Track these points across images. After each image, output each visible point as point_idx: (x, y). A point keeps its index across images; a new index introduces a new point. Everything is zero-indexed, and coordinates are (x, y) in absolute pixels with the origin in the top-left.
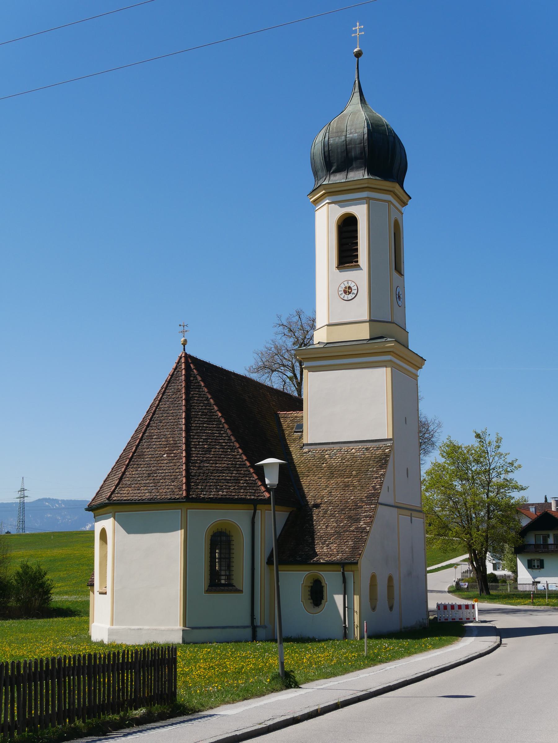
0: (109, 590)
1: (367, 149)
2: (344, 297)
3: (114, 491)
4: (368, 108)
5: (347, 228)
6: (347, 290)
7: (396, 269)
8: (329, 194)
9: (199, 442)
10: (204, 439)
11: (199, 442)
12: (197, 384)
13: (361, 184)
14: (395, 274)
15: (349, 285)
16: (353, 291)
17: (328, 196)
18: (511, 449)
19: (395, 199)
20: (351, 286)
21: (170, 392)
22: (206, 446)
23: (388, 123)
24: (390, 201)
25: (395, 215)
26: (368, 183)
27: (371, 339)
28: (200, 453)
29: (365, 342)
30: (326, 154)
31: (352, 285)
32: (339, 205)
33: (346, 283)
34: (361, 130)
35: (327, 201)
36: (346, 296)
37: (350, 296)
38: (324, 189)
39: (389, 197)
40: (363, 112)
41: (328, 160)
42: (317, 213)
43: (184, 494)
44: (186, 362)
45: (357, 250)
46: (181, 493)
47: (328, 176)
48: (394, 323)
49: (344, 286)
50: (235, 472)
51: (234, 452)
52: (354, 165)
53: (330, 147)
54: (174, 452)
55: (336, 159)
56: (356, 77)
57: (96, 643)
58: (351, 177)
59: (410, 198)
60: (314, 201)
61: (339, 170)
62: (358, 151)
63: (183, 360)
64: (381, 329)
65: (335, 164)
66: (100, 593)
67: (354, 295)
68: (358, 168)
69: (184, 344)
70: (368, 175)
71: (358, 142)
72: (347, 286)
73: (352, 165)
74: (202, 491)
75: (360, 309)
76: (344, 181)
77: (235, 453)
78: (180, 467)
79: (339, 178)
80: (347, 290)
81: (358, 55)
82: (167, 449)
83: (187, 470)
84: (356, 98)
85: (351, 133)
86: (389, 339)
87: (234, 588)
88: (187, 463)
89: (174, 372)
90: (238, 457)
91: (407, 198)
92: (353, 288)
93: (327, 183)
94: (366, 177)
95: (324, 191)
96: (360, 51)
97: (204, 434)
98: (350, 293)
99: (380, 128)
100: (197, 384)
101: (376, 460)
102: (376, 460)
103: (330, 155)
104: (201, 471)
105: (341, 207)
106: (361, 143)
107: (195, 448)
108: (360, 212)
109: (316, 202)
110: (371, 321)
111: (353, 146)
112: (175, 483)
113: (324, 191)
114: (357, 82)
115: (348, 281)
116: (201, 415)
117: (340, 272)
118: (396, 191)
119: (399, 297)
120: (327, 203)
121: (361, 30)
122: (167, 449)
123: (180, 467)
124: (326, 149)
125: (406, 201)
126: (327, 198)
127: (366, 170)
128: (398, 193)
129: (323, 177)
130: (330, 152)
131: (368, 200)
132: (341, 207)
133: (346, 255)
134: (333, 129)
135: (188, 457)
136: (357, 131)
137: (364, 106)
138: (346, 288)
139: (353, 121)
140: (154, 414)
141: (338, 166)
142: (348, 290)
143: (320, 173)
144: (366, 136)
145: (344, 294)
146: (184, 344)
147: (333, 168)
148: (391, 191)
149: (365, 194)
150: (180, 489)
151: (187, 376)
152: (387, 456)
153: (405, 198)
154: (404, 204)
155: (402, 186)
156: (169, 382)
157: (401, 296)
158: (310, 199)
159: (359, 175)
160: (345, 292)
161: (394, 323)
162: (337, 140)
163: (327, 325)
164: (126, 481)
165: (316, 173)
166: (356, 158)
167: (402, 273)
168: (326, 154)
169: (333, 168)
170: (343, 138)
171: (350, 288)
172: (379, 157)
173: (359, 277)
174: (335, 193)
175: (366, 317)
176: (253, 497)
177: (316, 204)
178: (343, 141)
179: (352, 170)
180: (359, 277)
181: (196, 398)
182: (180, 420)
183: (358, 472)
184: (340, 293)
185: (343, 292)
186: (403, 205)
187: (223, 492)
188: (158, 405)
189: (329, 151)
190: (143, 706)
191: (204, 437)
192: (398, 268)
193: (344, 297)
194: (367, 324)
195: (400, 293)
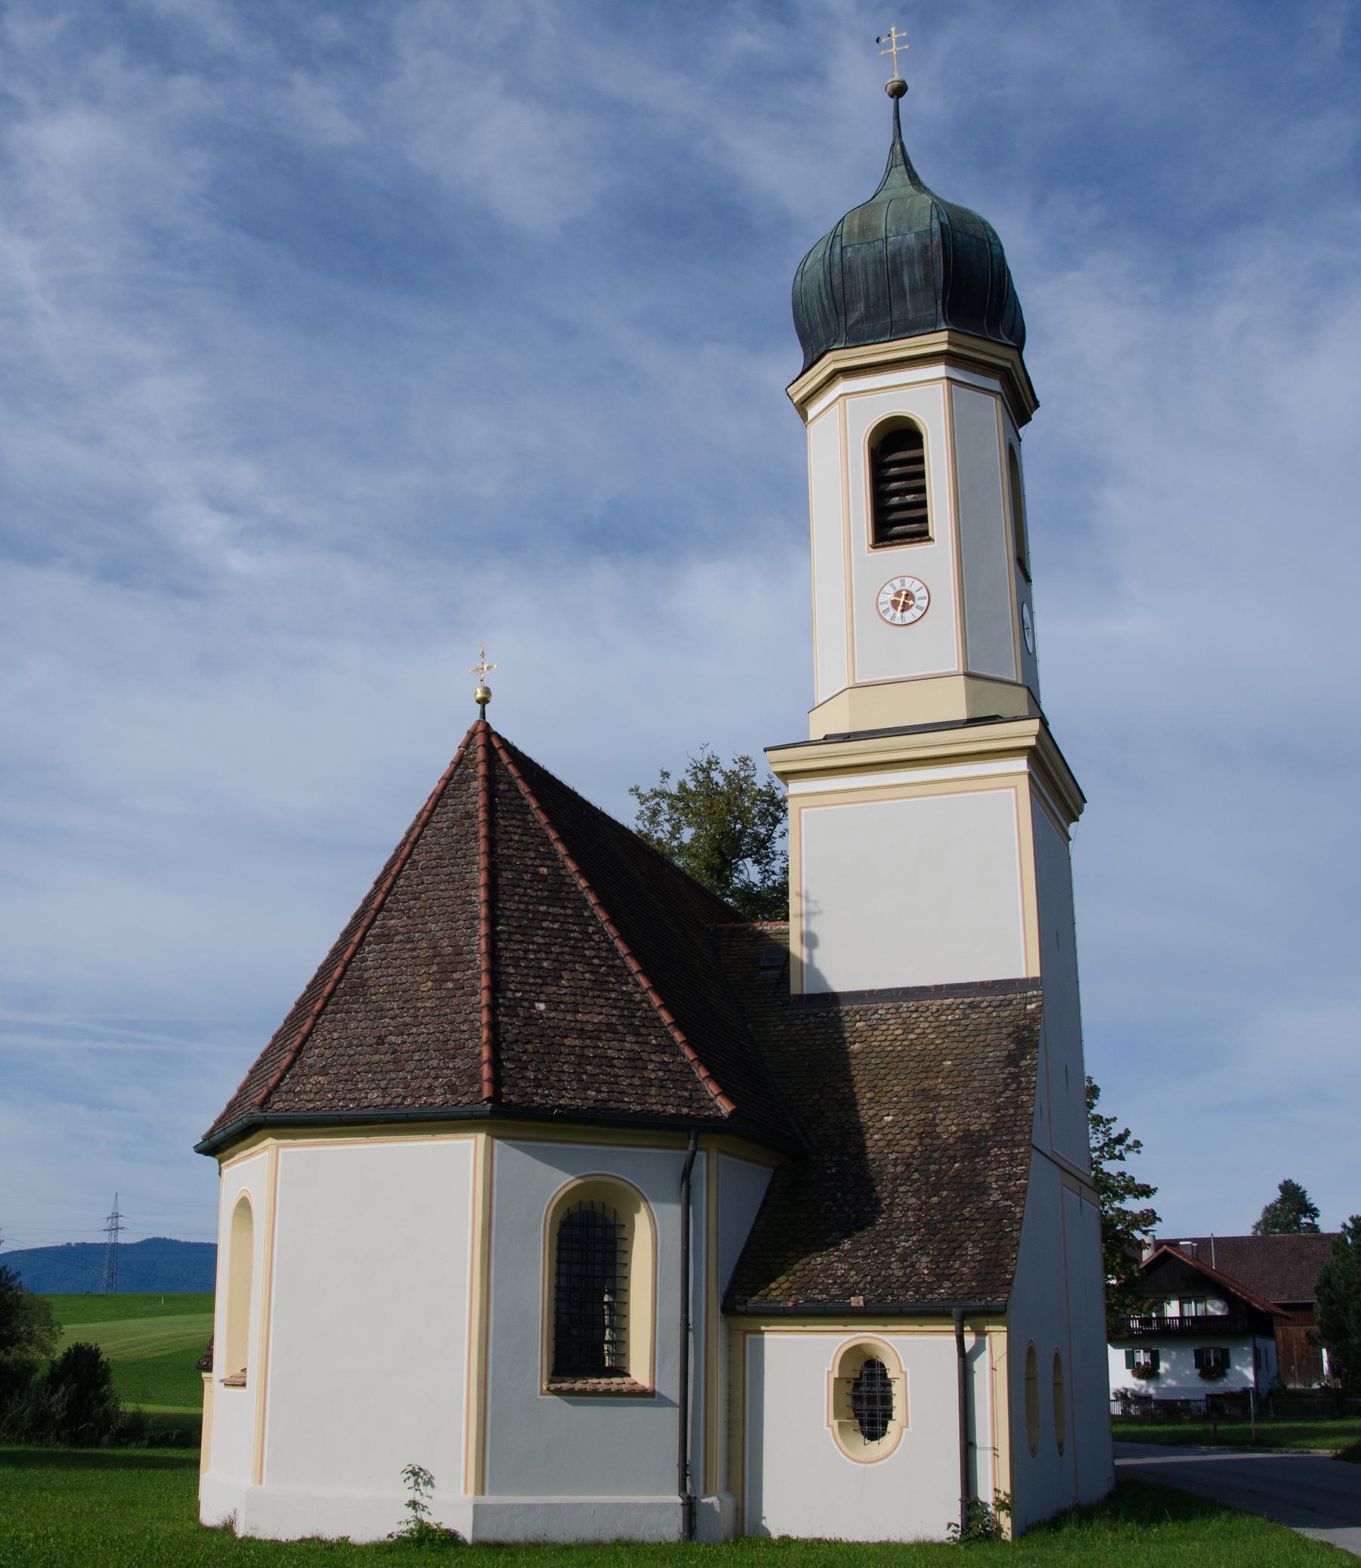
0: (252, 1378)
3: (277, 1085)
5: (895, 446)
9: (526, 951)
10: (539, 944)
11: (526, 951)
12: (518, 802)
15: (907, 586)
20: (913, 590)
21: (442, 821)
22: (545, 964)
28: (531, 980)
31: (913, 586)
33: (897, 583)
43: (487, 1091)
44: (488, 747)
46: (476, 1088)
50: (629, 1038)
51: (627, 983)
54: (456, 976)
57: (212, 1530)
63: (479, 740)
66: (229, 1384)
69: (484, 702)
74: (537, 1087)
75: (938, 643)
77: (630, 988)
78: (471, 1017)
82: (435, 968)
83: (494, 1026)
87: (626, 1379)
88: (493, 1007)
89: (455, 770)
90: (638, 997)
92: (917, 595)
97: (540, 932)
100: (518, 802)
101: (1004, 1031)
102: (1004, 1031)
104: (535, 1030)
107: (516, 967)
112: (458, 1062)
115: (902, 578)
116: (531, 881)
121: (900, 42)
122: (435, 968)
123: (471, 1017)
133: (896, 516)
135: (495, 988)
140: (397, 877)
142: (904, 601)
146: (484, 702)
150: (474, 1078)
151: (491, 780)
152: (1033, 1017)
156: (439, 799)
164: (311, 1058)
172: (967, 297)
173: (931, 564)
175: (956, 665)
176: (685, 1110)
181: (516, 837)
182: (473, 892)
183: (957, 1062)
184: (882, 608)
185: (889, 605)
187: (599, 1091)
188: (409, 855)
190: (1335, 1241)
191: (541, 941)
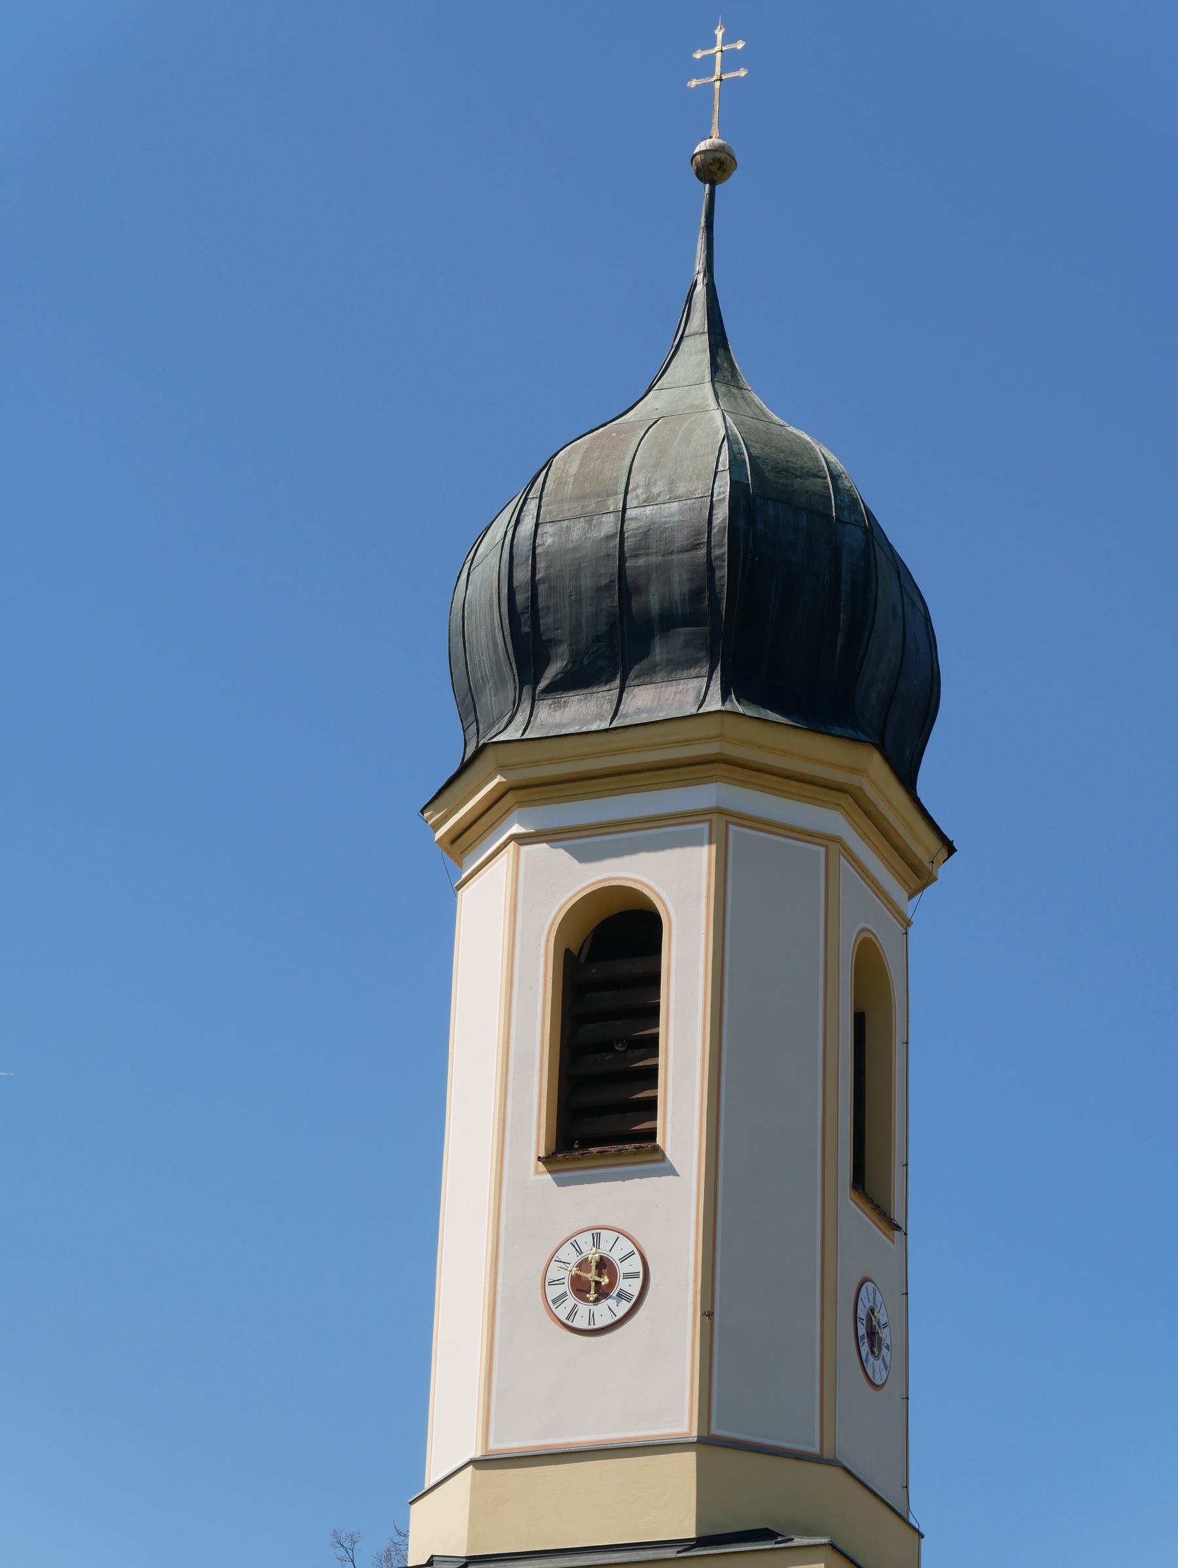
1: (722, 573)
2: (573, 1312)
4: (749, 402)
5: (607, 965)
6: (591, 1276)
7: (859, 1180)
8: (524, 791)
13: (688, 742)
14: (853, 1214)
15: (604, 1249)
16: (622, 1284)
17: (521, 803)
18: (570, 531)
19: (864, 836)
20: (615, 1256)
23: (840, 467)
24: (837, 840)
25: (860, 915)
26: (721, 737)
27: (702, 1541)
29: (671, 1553)
30: (521, 598)
32: (573, 852)
33: (585, 1241)
34: (700, 487)
35: (516, 829)
36: (583, 1309)
37: (604, 1313)
38: (502, 768)
39: (831, 820)
40: (718, 415)
41: (525, 629)
42: (467, 898)
45: (650, 1076)
47: (526, 706)
48: (833, 1463)
49: (574, 1259)
52: (658, 652)
53: (541, 565)
55: (572, 628)
56: (699, 266)
58: (639, 711)
59: (951, 849)
60: (456, 837)
61: (577, 679)
62: (679, 584)
64: (760, 1494)
65: (564, 649)
67: (625, 1306)
68: (676, 667)
70: (724, 699)
71: (681, 539)
72: (593, 1255)
73: (646, 652)
75: (654, 1378)
76: (605, 725)
79: (581, 712)
80: (591, 1276)
81: (714, 169)
84: (695, 354)
85: (649, 501)
86: (798, 1541)
91: (933, 843)
92: (622, 1268)
93: (518, 736)
94: (714, 703)
95: (499, 779)
96: (721, 149)
98: (603, 1293)
99: (797, 483)
103: (541, 603)
105: (582, 859)
106: (695, 547)
108: (678, 882)
109: (462, 841)
110: (707, 1442)
111: (655, 560)
113: (499, 779)
114: (700, 289)
117: (561, 1183)
118: (872, 794)
119: (872, 1334)
120: (515, 838)
121: (731, 60)
124: (522, 575)
125: (925, 860)
126: (516, 813)
127: (717, 675)
128: (883, 807)
129: (502, 716)
130: (541, 589)
131: (720, 825)
132: (583, 856)
133: (598, 1103)
134: (560, 483)
136: (682, 489)
137: (729, 394)
138: (583, 1265)
139: (665, 459)
141: (575, 657)
143: (489, 701)
144: (722, 513)
145: (571, 1300)
147: (553, 670)
148: (840, 789)
149: (704, 795)
153: (922, 845)
154: (919, 877)
155: (907, 777)
157: (884, 1334)
158: (436, 826)
159: (675, 696)
160: (579, 1287)
161: (833, 1463)
162: (575, 535)
163: (472, 1462)
165: (469, 707)
166: (669, 621)
167: (898, 1218)
168: (521, 598)
169: (553, 670)
170: (609, 524)
171: (604, 1265)
173: (658, 1213)
174: (554, 789)
175: (685, 1425)
177: (464, 852)
178: (609, 538)
179: (647, 676)
180: (658, 1213)
184: (553, 1292)
185: (566, 1288)
186: (915, 882)
189: (534, 584)
192: (870, 1171)
193: (573, 1312)
194: (689, 1459)
195: (881, 1316)
